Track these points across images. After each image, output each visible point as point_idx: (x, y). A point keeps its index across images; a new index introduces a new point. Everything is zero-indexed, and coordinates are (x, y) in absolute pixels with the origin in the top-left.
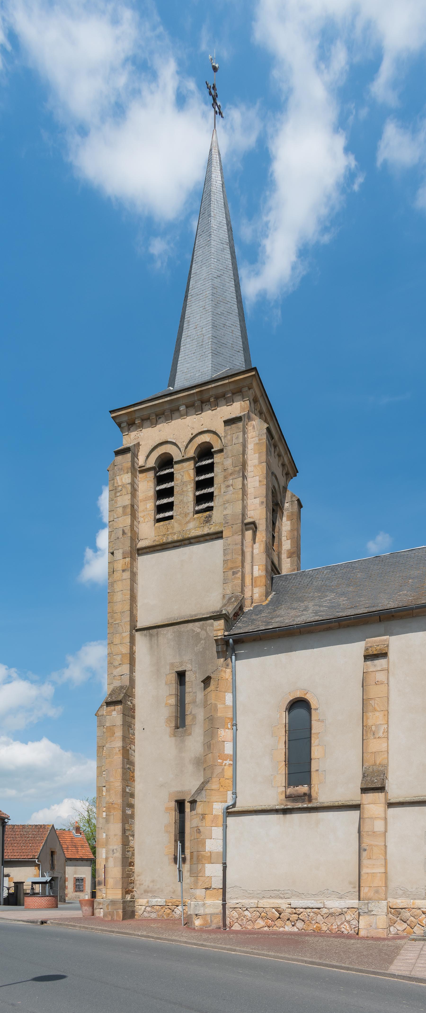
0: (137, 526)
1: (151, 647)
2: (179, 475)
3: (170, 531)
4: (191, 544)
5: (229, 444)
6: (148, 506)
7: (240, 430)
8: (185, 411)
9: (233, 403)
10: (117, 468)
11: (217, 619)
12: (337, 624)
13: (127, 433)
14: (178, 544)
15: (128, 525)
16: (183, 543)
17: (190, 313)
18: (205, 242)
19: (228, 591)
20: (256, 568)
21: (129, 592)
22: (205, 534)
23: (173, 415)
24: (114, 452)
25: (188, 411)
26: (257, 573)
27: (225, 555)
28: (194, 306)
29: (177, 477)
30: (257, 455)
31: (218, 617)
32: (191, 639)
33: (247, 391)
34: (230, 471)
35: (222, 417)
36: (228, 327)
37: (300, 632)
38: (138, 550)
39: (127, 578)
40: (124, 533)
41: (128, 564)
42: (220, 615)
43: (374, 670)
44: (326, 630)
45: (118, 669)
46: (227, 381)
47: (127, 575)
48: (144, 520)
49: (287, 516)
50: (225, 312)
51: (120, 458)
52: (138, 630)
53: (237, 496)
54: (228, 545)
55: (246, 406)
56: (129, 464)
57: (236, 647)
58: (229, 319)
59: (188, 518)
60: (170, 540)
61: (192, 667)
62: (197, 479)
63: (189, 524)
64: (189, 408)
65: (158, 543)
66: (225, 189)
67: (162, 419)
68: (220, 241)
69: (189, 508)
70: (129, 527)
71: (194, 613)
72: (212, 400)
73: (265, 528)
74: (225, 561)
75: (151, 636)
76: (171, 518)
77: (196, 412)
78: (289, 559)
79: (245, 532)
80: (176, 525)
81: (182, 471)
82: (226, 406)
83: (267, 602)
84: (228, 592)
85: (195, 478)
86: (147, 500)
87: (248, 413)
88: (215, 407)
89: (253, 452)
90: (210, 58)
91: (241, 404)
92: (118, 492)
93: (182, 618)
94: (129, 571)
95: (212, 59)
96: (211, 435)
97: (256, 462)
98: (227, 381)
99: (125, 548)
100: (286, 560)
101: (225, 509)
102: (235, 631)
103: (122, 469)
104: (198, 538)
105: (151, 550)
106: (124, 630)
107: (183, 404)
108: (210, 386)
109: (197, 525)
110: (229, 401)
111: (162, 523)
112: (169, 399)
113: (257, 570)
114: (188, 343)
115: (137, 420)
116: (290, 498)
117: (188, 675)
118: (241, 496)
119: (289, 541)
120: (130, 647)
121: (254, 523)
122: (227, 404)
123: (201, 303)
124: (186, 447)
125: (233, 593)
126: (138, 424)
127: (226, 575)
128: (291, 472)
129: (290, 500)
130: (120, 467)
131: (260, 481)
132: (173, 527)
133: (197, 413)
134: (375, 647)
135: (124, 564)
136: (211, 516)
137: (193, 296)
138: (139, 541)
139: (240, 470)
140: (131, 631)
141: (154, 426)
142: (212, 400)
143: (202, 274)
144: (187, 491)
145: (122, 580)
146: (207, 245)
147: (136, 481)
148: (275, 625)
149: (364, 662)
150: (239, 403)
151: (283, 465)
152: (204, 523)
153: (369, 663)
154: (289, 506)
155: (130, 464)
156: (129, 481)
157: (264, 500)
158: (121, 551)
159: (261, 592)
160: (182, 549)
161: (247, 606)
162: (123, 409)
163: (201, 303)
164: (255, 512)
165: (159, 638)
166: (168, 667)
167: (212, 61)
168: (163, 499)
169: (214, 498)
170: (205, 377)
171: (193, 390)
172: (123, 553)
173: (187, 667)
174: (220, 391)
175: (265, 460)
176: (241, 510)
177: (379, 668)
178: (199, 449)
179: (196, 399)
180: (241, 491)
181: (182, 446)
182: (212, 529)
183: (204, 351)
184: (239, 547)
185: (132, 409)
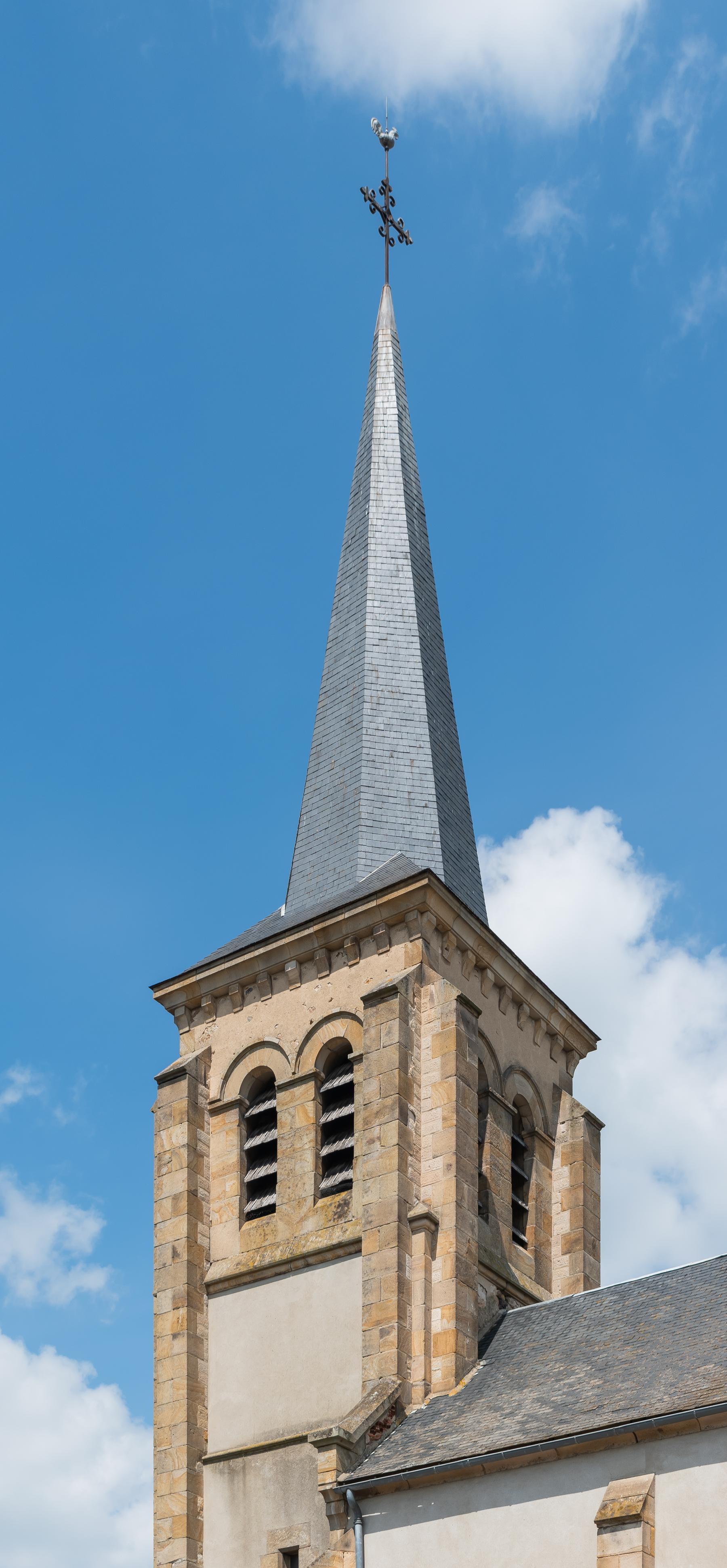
0: (207, 1233)
1: (233, 1497)
2: (287, 1114)
3: (270, 1239)
4: (308, 1266)
5: (374, 1048)
6: (227, 1186)
7: (394, 1016)
8: (297, 973)
9: (390, 947)
10: (161, 1114)
11: (324, 1448)
12: (552, 1451)
13: (187, 1029)
14: (283, 1269)
15: (182, 1236)
16: (292, 1265)
17: (321, 735)
18: (356, 562)
19: (372, 1373)
20: (436, 1314)
21: (185, 1382)
22: (334, 1245)
23: (274, 982)
24: (155, 1079)
25: (304, 970)
26: (439, 1326)
27: (365, 1293)
28: (330, 718)
29: (283, 1119)
30: (438, 1060)
31: (324, 1444)
32: (307, 1478)
33: (416, 919)
34: (375, 1107)
35: (369, 979)
36: (400, 755)
37: (484, 1469)
38: (208, 1285)
39: (183, 1351)
40: (175, 1254)
41: (182, 1322)
42: (328, 1439)
43: (617, 1552)
44: (534, 1465)
45: (166, 1550)
46: (373, 904)
47: (181, 1345)
48: (220, 1218)
49: (563, 1154)
50: (394, 721)
51: (167, 1090)
52: (206, 1462)
53: (388, 1162)
54: (371, 1272)
55: (416, 951)
56: (184, 1104)
57: (363, 1505)
58: (405, 736)
59: (305, 1209)
60: (267, 1261)
61: (310, 1538)
62: (323, 1120)
63: (306, 1222)
64: (306, 965)
65: (244, 1269)
66: (406, 422)
67: (254, 993)
68: (389, 554)
69: (307, 1187)
70: (184, 1242)
71: (315, 1420)
72: (348, 944)
73: (454, 1223)
74: (367, 1307)
75: (232, 1472)
76: (270, 1209)
77: (319, 972)
78: (567, 1256)
79: (410, 1238)
80: (281, 1225)
81: (292, 1105)
82: (376, 956)
83: (460, 1388)
84: (373, 1375)
85: (317, 1118)
86: (225, 1174)
87: (421, 967)
88: (356, 958)
89: (430, 1053)
90: (372, 126)
91: (406, 947)
92: (165, 1165)
93: (292, 1432)
94: (186, 1335)
95: (378, 125)
96: (348, 1021)
97: (436, 1075)
98: (373, 904)
99: (178, 1287)
100: (559, 1259)
101: (366, 1192)
102: (368, 1469)
103: (171, 1115)
104: (323, 1254)
105: (232, 1284)
106: (177, 1465)
107: (291, 959)
108: (341, 918)
109: (321, 1223)
110: (384, 944)
111: (255, 1222)
112: (262, 951)
113: (440, 1317)
114: (315, 806)
115: (204, 999)
116: (568, 1112)
117: (302, 1556)
118: (395, 1161)
119: (567, 1215)
120: (188, 1500)
121: (427, 1216)
122: (378, 949)
123: (343, 710)
124: (299, 1053)
125: (380, 1378)
126: (207, 1009)
127: (368, 1338)
128: (576, 1044)
129: (568, 1117)
130: (167, 1110)
131: (444, 1119)
132: (274, 1232)
133: (320, 975)
134: (622, 1500)
135: (176, 1320)
136: (349, 1203)
137: (329, 693)
138: (211, 1264)
139: (394, 1103)
140: (190, 1466)
141: (238, 1009)
142: (348, 944)
143: (347, 641)
144: (302, 1149)
145: (172, 1356)
146: (360, 571)
147: (202, 1135)
148: (448, 1455)
149: (598, 1534)
150: (403, 945)
151: (552, 1035)
152: (334, 1219)
153: (607, 1536)
154: (567, 1131)
155: (187, 1102)
156: (184, 1139)
157: (453, 1160)
158: (169, 1293)
159: (447, 1367)
160: (291, 1278)
161: (416, 1401)
162: (176, 980)
163: (343, 710)
164: (434, 1187)
165: (248, 1477)
166: (264, 1540)
167: (380, 129)
168: (340, 1107)
169: (354, 1161)
170: (345, 884)
171: (308, 928)
172: (174, 1298)
173: (300, 1539)
174: (363, 924)
175: (454, 1072)
176: (397, 1193)
177: (626, 1549)
178: (328, 1052)
179: (316, 945)
180: (397, 1151)
181: (291, 1049)
182: (348, 1233)
183: (346, 822)
184: (393, 1274)
185: (193, 979)
